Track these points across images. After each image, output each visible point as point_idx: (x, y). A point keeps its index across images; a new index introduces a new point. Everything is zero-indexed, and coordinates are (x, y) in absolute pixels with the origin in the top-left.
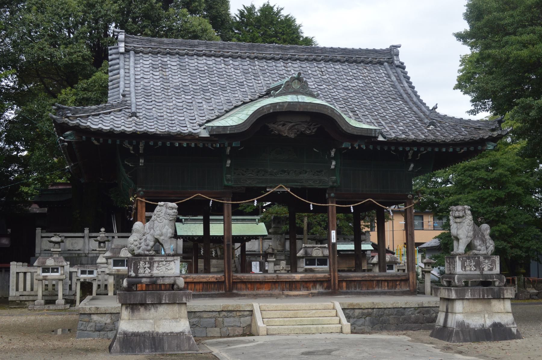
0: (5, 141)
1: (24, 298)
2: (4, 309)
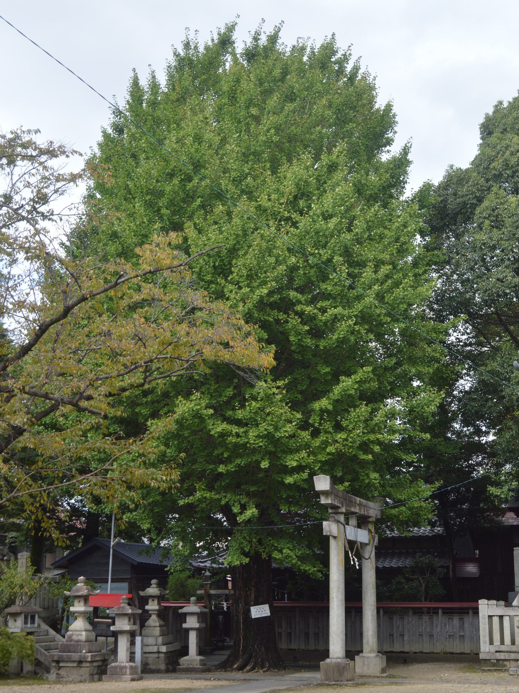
0: (461, 421)
1: (502, 656)
2: (475, 672)
